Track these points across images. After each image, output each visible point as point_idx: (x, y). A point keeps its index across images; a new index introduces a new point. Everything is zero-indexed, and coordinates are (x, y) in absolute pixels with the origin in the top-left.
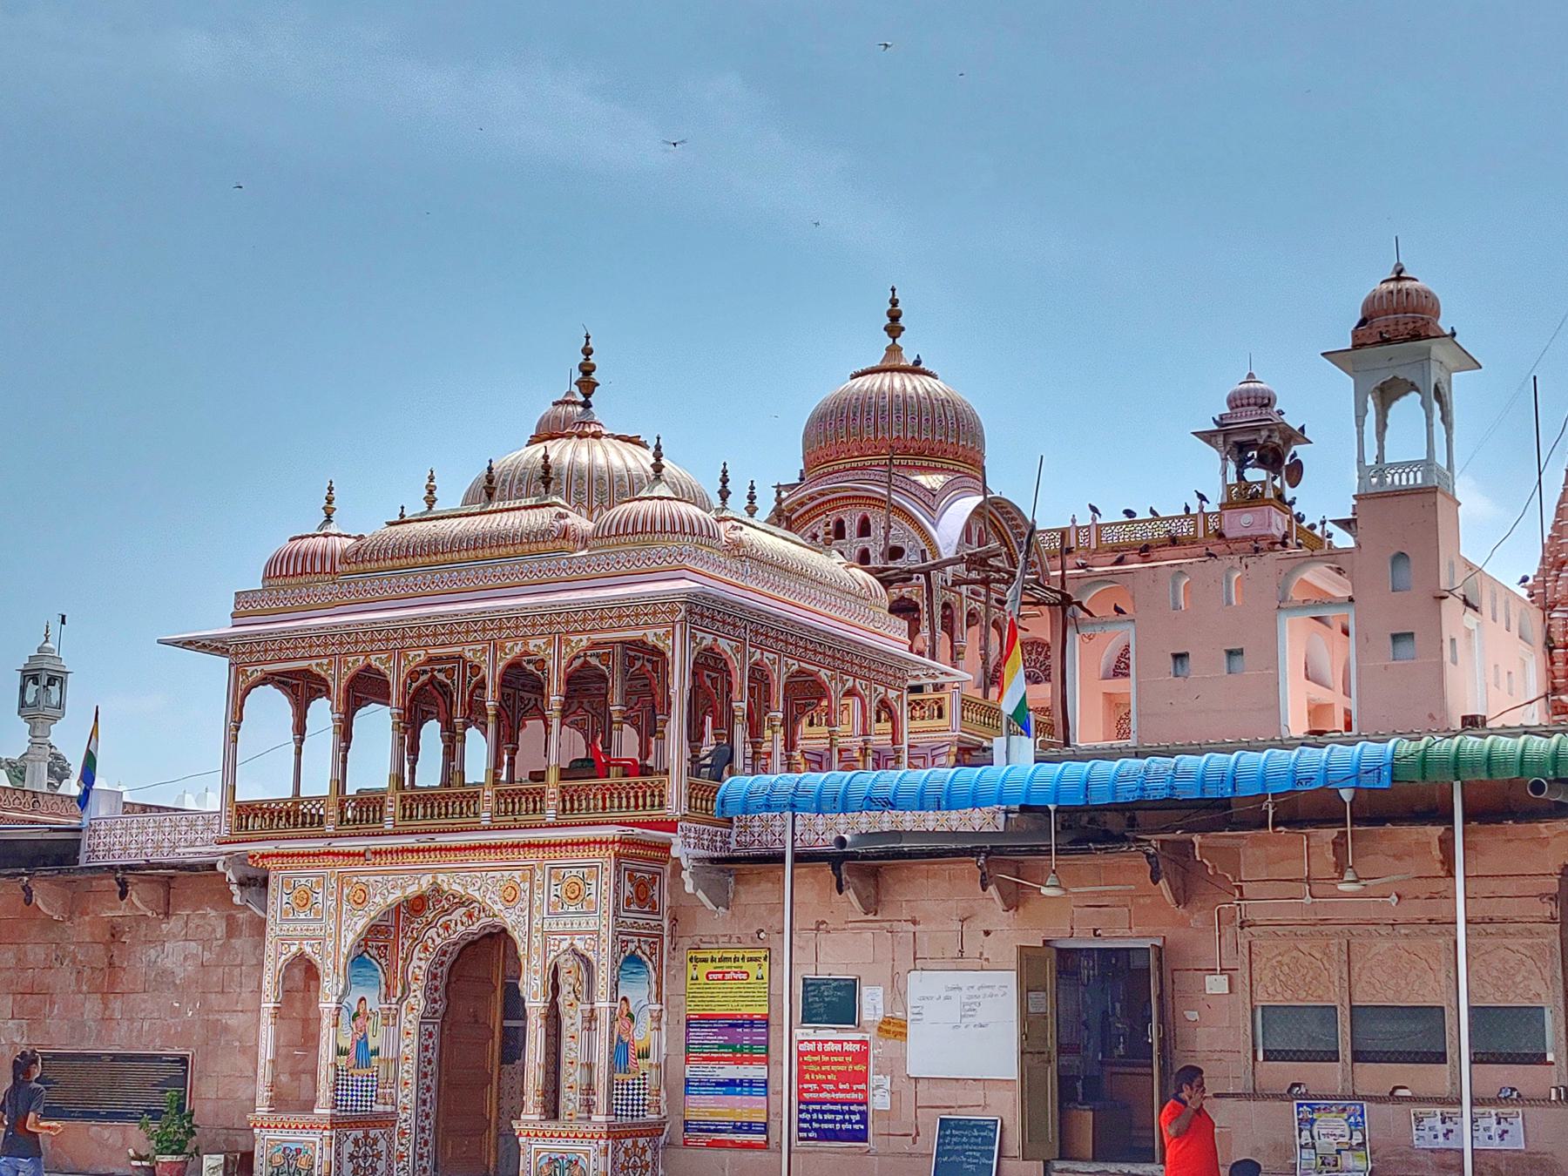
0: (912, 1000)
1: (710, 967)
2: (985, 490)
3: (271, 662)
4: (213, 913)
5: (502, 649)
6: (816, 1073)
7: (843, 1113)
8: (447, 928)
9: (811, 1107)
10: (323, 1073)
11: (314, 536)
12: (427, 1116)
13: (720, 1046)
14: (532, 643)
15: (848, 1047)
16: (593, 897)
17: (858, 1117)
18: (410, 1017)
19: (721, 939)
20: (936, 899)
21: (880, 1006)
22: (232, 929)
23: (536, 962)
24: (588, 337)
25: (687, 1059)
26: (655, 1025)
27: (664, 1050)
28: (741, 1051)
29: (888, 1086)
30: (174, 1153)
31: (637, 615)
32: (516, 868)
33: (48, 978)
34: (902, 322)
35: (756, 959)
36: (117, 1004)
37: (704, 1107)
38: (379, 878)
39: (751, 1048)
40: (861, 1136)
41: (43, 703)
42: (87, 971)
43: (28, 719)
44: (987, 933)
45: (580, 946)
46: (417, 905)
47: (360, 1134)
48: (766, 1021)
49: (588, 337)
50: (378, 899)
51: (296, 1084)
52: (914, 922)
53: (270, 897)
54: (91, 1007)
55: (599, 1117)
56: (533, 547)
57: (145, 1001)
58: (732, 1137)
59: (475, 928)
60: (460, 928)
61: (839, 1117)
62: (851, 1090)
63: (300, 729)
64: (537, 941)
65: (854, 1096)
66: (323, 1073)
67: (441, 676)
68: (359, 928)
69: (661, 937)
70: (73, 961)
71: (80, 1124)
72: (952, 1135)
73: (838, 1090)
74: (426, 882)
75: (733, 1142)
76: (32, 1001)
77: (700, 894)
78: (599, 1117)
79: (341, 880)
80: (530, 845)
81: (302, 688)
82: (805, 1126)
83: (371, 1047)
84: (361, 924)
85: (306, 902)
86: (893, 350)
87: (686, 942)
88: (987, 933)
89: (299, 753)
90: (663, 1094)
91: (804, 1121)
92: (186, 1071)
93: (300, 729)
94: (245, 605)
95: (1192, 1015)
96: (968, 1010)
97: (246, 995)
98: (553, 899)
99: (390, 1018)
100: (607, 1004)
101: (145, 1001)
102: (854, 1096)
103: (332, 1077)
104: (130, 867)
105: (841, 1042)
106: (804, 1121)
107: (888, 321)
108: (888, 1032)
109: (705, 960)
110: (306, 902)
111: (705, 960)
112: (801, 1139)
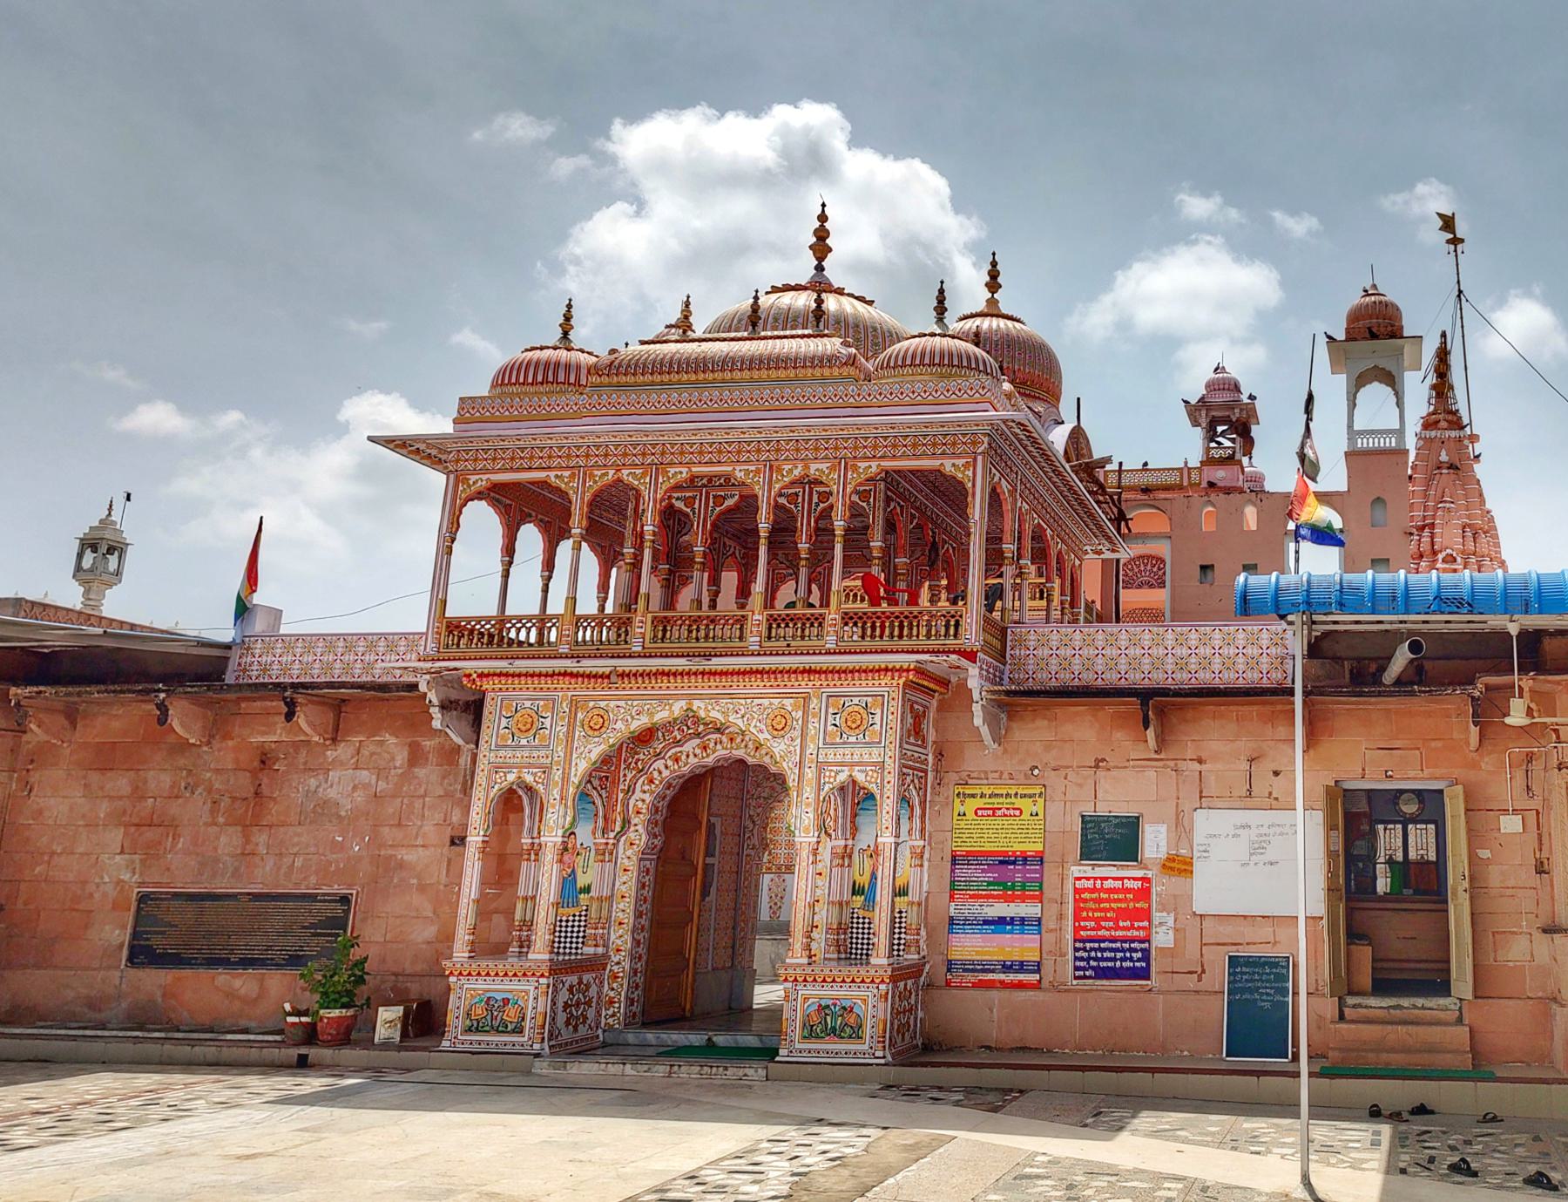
0: (1199, 837)
1: (979, 803)
2: (1453, 232)
3: (501, 470)
4: (393, 740)
5: (779, 470)
6: (1094, 910)
7: (1123, 950)
8: (677, 760)
9: (1088, 945)
10: (543, 914)
11: (555, 348)
12: (640, 958)
13: (989, 884)
14: (813, 467)
15: (1129, 884)
16: (877, 727)
17: (1139, 955)
18: (629, 853)
19: (991, 775)
20: (1218, 742)
21: (1163, 843)
22: (416, 756)
23: (809, 792)
24: (824, 205)
25: (952, 897)
26: (918, 862)
27: (925, 888)
28: (1013, 889)
29: (1171, 923)
30: (343, 1006)
31: (934, 445)
32: (789, 696)
33: (174, 809)
34: (999, 280)
35: (1030, 796)
36: (261, 839)
37: (969, 946)
38: (622, 703)
39: (1024, 889)
40: (1144, 974)
41: (100, 569)
42: (225, 802)
43: (83, 582)
44: (1276, 773)
45: (860, 777)
46: (645, 737)
47: (573, 979)
48: (1040, 858)
49: (824, 205)
50: (619, 725)
51: (485, 924)
52: (1200, 761)
53: (484, 727)
54: (228, 842)
55: (880, 959)
56: (818, 372)
57: (299, 835)
58: (1002, 976)
59: (710, 760)
60: (692, 760)
61: (1119, 955)
62: (1132, 927)
63: (509, 551)
64: (810, 774)
65: (1136, 933)
66: (543, 914)
67: (679, 505)
68: (594, 756)
69: (926, 772)
70: (209, 791)
71: (204, 973)
72: (1243, 973)
73: (1118, 928)
74: (678, 707)
75: (1002, 982)
76: (150, 834)
77: (985, 731)
78: (880, 959)
79: (575, 705)
80: (810, 671)
81: (524, 504)
82: (1082, 964)
83: (580, 884)
84: (596, 750)
85: (531, 726)
86: (992, 302)
87: (953, 777)
88: (1276, 773)
89: (506, 575)
90: (923, 933)
91: (1082, 959)
92: (347, 912)
93: (509, 551)
94: (468, 411)
95: (1484, 854)
96: (1257, 848)
97: (428, 828)
98: (830, 728)
99: (606, 854)
100: (892, 840)
101: (299, 835)
102: (1136, 933)
103: (551, 919)
104: (304, 685)
105: (1122, 879)
106: (1082, 959)
107: (988, 278)
108: (1172, 869)
109: (973, 796)
110: (531, 726)
111: (973, 796)
112: (1076, 978)
